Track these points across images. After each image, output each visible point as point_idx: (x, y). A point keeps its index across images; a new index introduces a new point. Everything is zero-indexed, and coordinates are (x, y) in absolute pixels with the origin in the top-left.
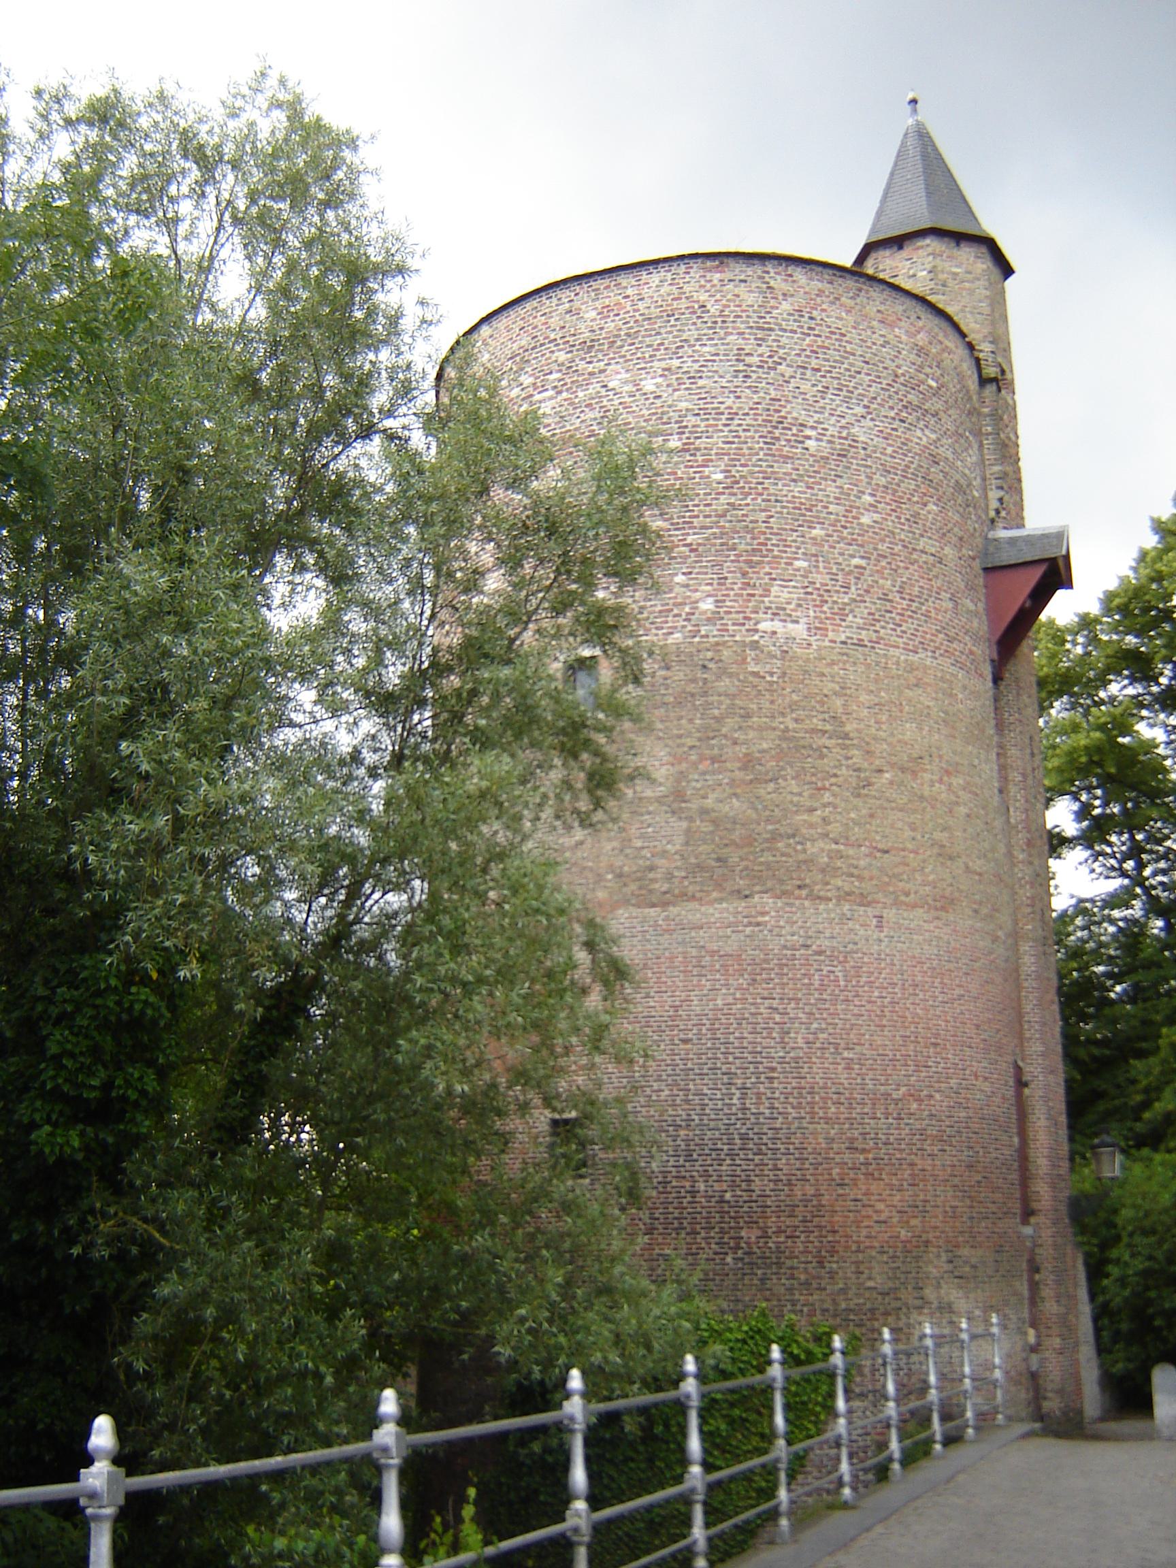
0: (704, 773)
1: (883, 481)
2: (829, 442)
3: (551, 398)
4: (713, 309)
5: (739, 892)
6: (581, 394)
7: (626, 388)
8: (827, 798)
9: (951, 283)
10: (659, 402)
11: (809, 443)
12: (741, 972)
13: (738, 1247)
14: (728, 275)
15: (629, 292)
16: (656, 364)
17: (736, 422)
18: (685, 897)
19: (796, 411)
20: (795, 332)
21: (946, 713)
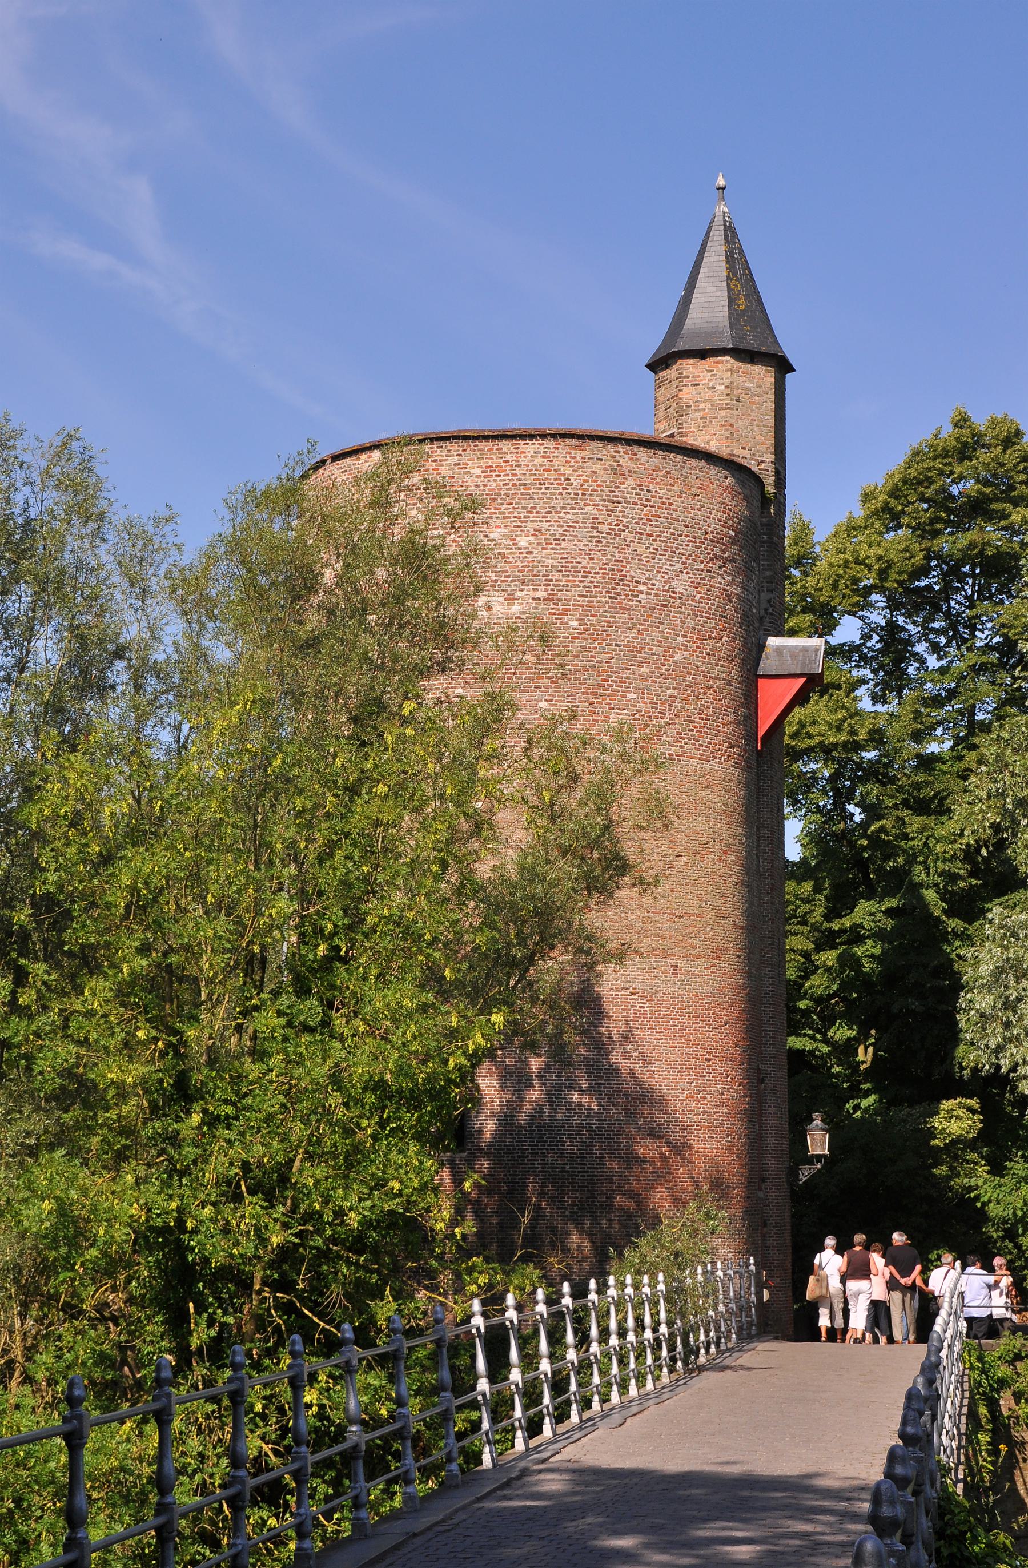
1: (692, 624)
2: (656, 595)
4: (576, 483)
10: (530, 557)
11: (642, 597)
14: (586, 454)
15: (509, 457)
19: (632, 570)
20: (635, 504)
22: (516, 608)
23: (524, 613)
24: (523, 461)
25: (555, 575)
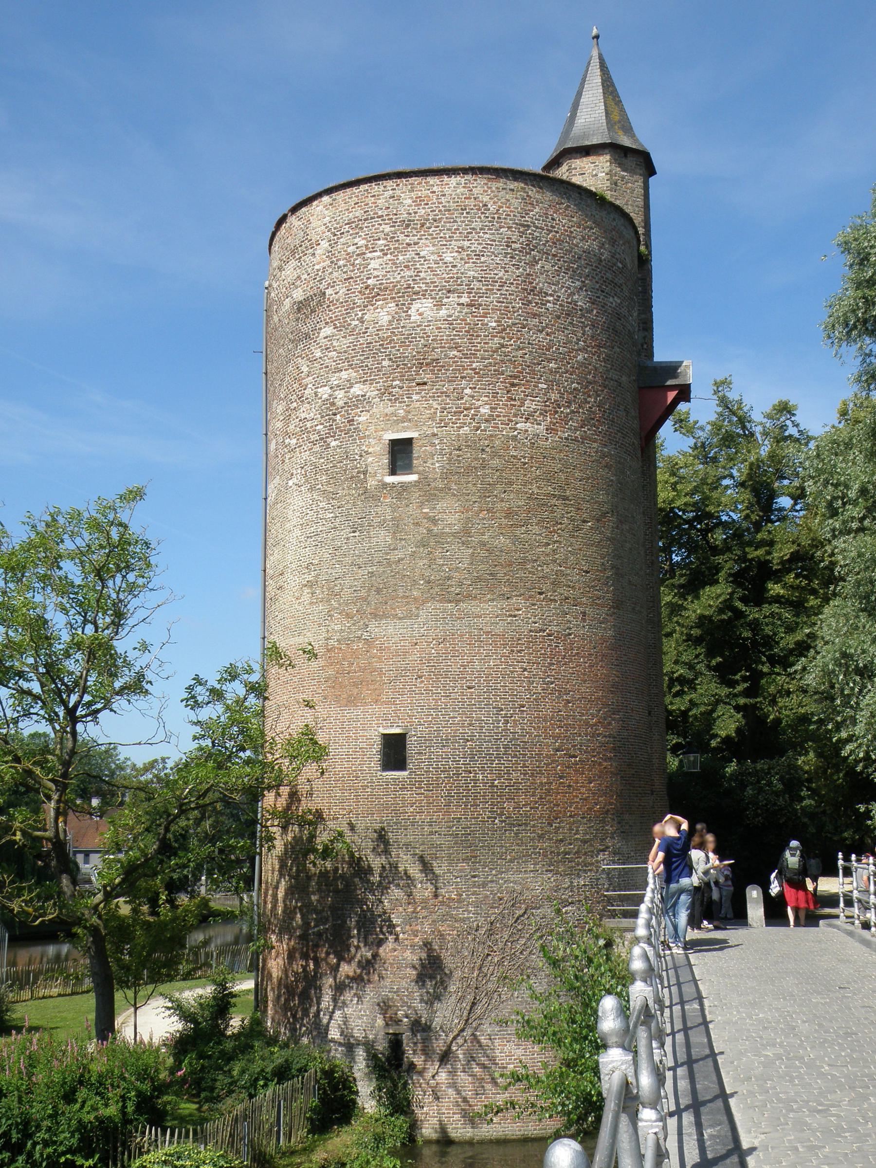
0: (484, 519)
3: (379, 257)
4: (492, 208)
5: (503, 595)
6: (401, 258)
7: (432, 257)
8: (556, 537)
9: (619, 183)
12: (505, 645)
13: (502, 814)
15: (435, 189)
16: (453, 243)
17: (505, 288)
18: (469, 597)
21: (621, 484)
22: (443, 312)
23: (450, 316)
24: (447, 191)
25: (476, 285)
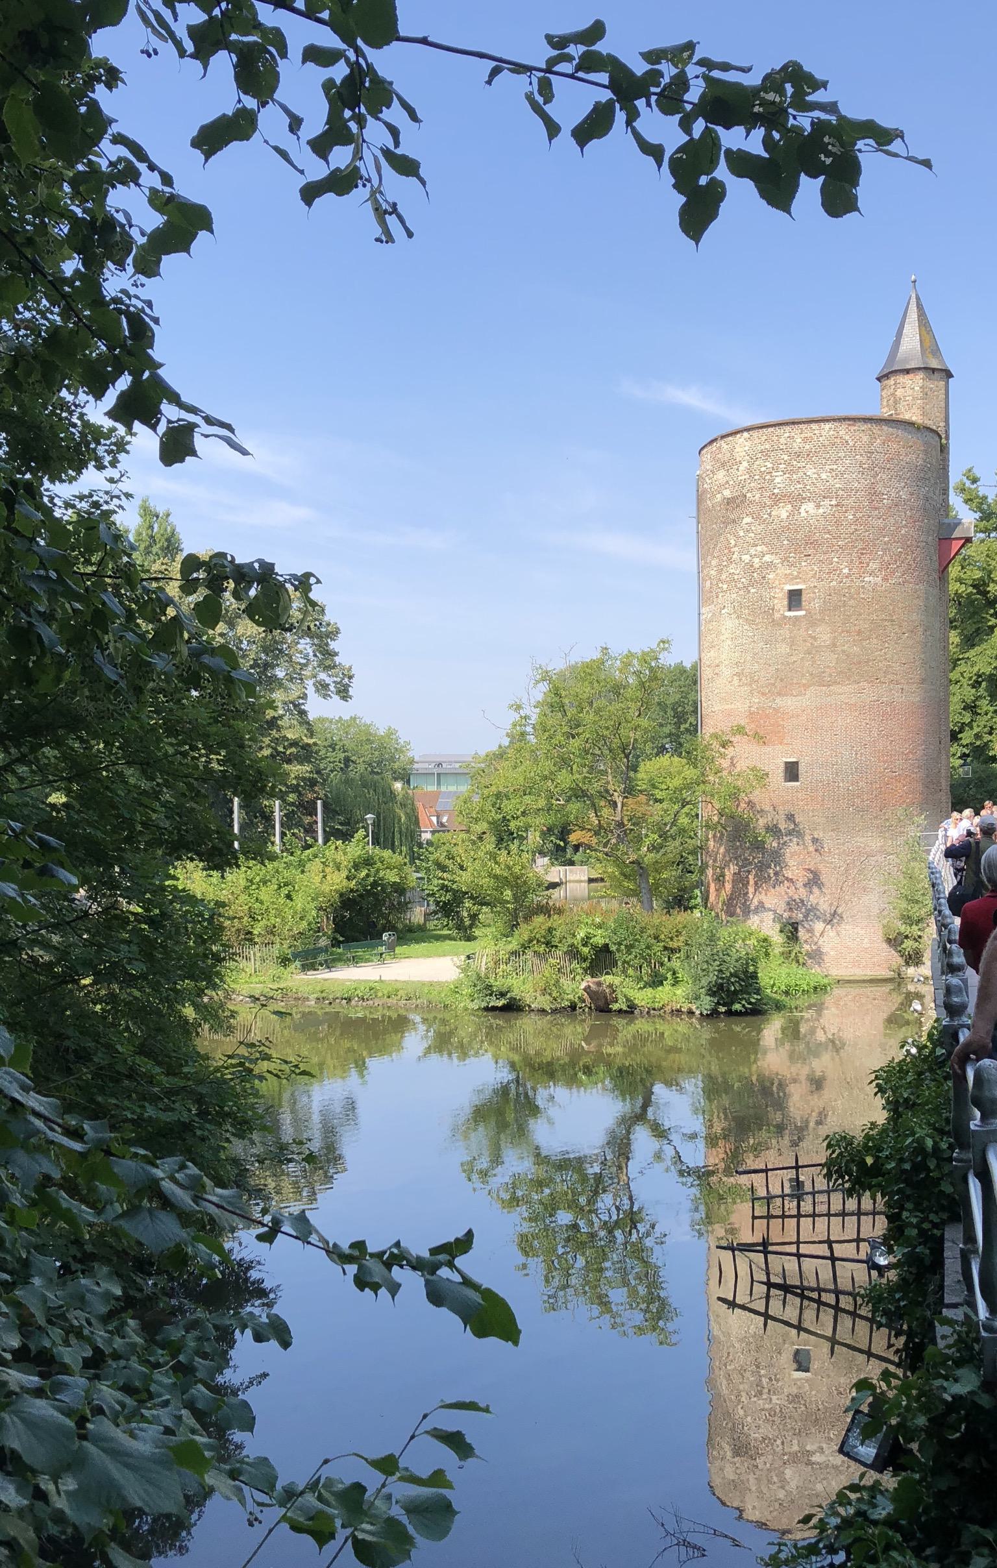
18: (835, 683)
19: (879, 488)
22: (821, 511)
24: (824, 434)
